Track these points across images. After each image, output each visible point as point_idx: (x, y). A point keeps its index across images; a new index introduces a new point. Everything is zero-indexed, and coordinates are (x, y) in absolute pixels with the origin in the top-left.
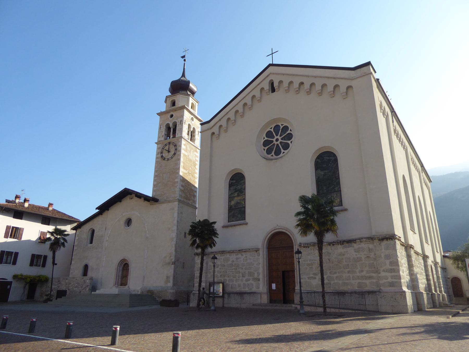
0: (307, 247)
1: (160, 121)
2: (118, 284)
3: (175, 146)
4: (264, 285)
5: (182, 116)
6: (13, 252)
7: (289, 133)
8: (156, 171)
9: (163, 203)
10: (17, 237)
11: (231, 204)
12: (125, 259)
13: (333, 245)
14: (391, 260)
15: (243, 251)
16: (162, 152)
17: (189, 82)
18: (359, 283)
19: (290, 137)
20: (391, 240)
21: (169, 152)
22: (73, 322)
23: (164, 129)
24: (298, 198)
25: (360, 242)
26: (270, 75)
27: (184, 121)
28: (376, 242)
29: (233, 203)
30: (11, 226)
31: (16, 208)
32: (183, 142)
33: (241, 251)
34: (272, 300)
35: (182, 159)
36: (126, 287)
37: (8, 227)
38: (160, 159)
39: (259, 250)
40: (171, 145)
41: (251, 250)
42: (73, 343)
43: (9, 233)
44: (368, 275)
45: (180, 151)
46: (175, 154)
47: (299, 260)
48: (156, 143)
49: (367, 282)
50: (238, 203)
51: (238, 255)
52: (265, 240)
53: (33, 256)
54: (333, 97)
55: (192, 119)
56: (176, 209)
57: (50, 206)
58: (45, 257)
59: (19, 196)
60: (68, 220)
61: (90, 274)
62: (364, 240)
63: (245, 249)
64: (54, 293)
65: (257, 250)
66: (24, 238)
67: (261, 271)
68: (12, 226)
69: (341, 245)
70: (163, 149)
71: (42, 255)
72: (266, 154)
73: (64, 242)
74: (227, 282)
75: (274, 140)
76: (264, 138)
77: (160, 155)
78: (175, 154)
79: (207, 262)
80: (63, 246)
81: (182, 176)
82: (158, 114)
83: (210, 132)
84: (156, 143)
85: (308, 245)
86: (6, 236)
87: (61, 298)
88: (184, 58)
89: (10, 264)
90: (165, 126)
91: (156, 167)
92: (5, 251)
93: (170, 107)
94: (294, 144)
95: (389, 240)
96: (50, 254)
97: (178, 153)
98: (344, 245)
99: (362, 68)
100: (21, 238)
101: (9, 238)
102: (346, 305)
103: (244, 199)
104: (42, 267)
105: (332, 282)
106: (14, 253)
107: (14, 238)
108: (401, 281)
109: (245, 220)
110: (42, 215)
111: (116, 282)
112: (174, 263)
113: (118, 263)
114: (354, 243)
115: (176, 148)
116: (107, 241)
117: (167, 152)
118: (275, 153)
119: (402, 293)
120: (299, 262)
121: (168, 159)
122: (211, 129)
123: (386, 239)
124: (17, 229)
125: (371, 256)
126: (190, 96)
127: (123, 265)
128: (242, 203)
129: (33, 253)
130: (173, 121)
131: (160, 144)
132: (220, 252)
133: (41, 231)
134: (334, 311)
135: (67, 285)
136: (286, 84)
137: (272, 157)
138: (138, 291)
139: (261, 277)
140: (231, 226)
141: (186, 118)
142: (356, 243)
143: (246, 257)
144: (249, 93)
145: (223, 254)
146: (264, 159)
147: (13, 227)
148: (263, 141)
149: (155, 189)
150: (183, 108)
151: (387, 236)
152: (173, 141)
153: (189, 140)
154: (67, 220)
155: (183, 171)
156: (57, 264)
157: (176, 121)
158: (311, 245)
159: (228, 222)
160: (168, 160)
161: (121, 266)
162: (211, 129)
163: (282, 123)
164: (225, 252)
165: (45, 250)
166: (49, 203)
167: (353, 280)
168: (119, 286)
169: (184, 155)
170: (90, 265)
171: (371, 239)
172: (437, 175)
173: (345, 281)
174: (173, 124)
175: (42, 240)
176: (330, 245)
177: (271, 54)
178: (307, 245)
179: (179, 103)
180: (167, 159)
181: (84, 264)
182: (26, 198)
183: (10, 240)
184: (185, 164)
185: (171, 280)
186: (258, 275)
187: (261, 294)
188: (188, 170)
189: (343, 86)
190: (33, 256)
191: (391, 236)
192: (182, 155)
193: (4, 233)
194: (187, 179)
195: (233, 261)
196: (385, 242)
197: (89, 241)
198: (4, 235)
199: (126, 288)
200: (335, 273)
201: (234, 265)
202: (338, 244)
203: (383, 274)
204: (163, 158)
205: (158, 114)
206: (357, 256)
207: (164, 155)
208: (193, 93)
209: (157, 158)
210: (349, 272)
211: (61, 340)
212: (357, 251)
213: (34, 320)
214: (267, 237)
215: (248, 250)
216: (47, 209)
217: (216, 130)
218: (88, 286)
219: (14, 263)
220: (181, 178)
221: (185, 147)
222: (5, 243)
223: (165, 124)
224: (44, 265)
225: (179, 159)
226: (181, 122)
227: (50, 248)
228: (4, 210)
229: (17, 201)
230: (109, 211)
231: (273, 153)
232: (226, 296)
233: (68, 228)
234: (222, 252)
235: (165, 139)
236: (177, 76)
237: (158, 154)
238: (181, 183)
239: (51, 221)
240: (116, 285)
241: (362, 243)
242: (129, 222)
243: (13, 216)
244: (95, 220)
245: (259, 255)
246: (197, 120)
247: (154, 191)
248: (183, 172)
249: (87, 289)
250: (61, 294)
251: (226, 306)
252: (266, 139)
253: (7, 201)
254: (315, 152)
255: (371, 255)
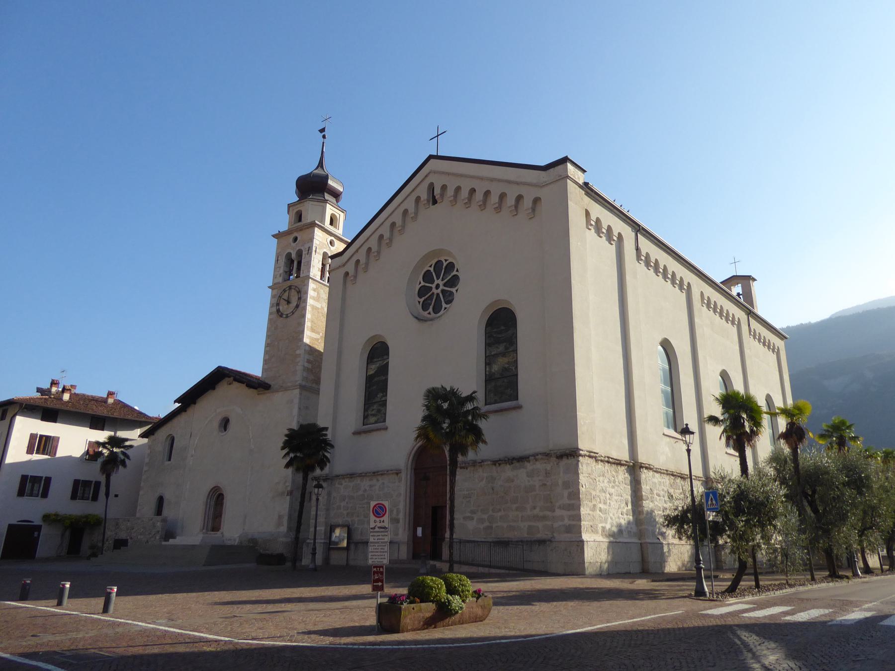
0: (464, 468)
1: (277, 248)
2: (207, 529)
3: (299, 292)
4: (405, 530)
5: (311, 240)
6: (42, 477)
7: (454, 276)
8: (268, 337)
9: (277, 391)
10: (49, 451)
11: (493, 371)
12: (217, 486)
13: (500, 464)
14: (570, 490)
15: (379, 473)
16: (279, 304)
17: (326, 178)
18: (530, 527)
19: (454, 281)
20: (572, 457)
21: (288, 302)
22: (30, 579)
23: (283, 263)
24: (423, 391)
25: (535, 460)
26: (431, 175)
27: (314, 249)
28: (554, 459)
29: (495, 368)
30: (37, 435)
31: (45, 405)
32: (312, 285)
33: (376, 474)
34: (415, 555)
35: (308, 316)
36: (219, 534)
37: (33, 437)
38: (275, 316)
39: (401, 472)
40: (293, 290)
41: (390, 472)
42: (172, 630)
43: (39, 442)
44: (541, 514)
45: (305, 301)
46: (297, 306)
47: (318, 497)
48: (269, 287)
49: (540, 525)
50: (505, 370)
51: (372, 480)
52: (410, 456)
53: (76, 483)
54: (516, 215)
55: (332, 243)
56: (296, 401)
57: (110, 396)
58: (98, 484)
59: (57, 381)
60: (133, 419)
61: (166, 512)
62: (540, 457)
63: (381, 471)
64: (109, 543)
65: (398, 473)
66: (61, 452)
67: (401, 506)
68: (40, 433)
69: (510, 464)
70: (281, 297)
71: (92, 482)
72: (421, 310)
73: (124, 459)
74: (356, 525)
75: (434, 286)
76: (420, 283)
77: (274, 309)
78: (297, 306)
79: (330, 492)
80: (122, 466)
81: (308, 345)
82: (274, 236)
83: (342, 272)
84: (269, 287)
85: (465, 464)
86: (30, 451)
87: (120, 549)
88: (323, 133)
89: (37, 496)
90: (284, 257)
91: (269, 330)
92: (28, 476)
93: (294, 223)
94: (461, 293)
95: (569, 458)
96: (102, 479)
97: (302, 305)
98: (514, 464)
99: (556, 168)
100: (55, 454)
101: (36, 454)
102: (509, 562)
103: (516, 362)
104: (92, 500)
105: (494, 525)
106: (44, 478)
107: (43, 454)
108: (582, 525)
109: (517, 399)
110: (90, 414)
111: (204, 526)
112: (290, 493)
113: (208, 493)
114: (527, 461)
115: (299, 296)
116: (192, 456)
117: (286, 302)
118: (433, 309)
119: (580, 543)
120: (317, 499)
121: (287, 314)
122: (344, 265)
123: (566, 457)
124: (48, 438)
125: (548, 483)
126: (327, 203)
127: (215, 496)
128: (512, 370)
129: (52, 479)
130: (298, 249)
131: (277, 288)
132: (349, 476)
133: (89, 441)
134: (483, 571)
135: (128, 531)
136: (450, 192)
137: (429, 316)
138: (235, 540)
139: (401, 516)
140: (365, 432)
141: (318, 243)
142: (529, 461)
143: (383, 483)
144: (399, 205)
145: (351, 478)
146: (415, 319)
147: (41, 436)
148: (418, 287)
149: (266, 367)
150: (313, 225)
151: (568, 452)
152: (295, 285)
153: (325, 282)
154: (134, 421)
155: (310, 335)
156: (114, 495)
157: (302, 248)
158: (471, 464)
159: (363, 425)
160: (287, 316)
161: (213, 498)
162: (344, 265)
163: (447, 258)
164: (355, 476)
165: (93, 472)
166: (109, 392)
167: (522, 521)
168: (209, 533)
169: (313, 307)
170: (167, 497)
171: (547, 455)
172: (885, 307)
173: (511, 524)
174: (297, 253)
175: (92, 455)
176: (495, 465)
177: (440, 134)
178: (464, 465)
179: (307, 218)
180: (284, 316)
181: (157, 495)
182: (65, 384)
183: (36, 457)
184: (315, 324)
185: (285, 521)
186: (398, 514)
187: (399, 544)
188: (321, 334)
189: (529, 196)
190: (76, 483)
191: (572, 451)
192: (309, 308)
193: (27, 446)
194: (318, 349)
195: (365, 490)
196: (565, 461)
197: (166, 457)
198: (26, 448)
199: (216, 535)
200: (500, 510)
201: (366, 496)
202: (506, 463)
203: (558, 512)
204: (280, 314)
205: (274, 236)
206: (530, 484)
207: (281, 308)
208: (336, 195)
209: (270, 314)
210: (517, 509)
211: (9, 603)
212: (530, 475)
213: (28, 582)
214: (412, 450)
215: (386, 472)
216: (104, 401)
217: (350, 268)
218: (158, 532)
219: (45, 495)
220: (307, 348)
221: (316, 293)
222: (30, 462)
223: (285, 254)
224: (95, 498)
225: (304, 316)
226: (309, 250)
227: (101, 469)
228: (25, 408)
229: (54, 389)
230: (196, 405)
231: (431, 310)
232: (352, 547)
233: (133, 436)
234: (350, 475)
235: (285, 281)
236: (308, 167)
237: (272, 306)
238: (307, 357)
239: (106, 424)
240: (204, 531)
241: (537, 463)
242: (225, 424)
243: (40, 417)
244: (176, 421)
245: (400, 481)
246: (342, 243)
247: (264, 370)
248: (312, 339)
249: (157, 538)
250: (120, 544)
251: (352, 563)
252: (423, 284)
253: (39, 390)
254: (487, 308)
255: (547, 482)
